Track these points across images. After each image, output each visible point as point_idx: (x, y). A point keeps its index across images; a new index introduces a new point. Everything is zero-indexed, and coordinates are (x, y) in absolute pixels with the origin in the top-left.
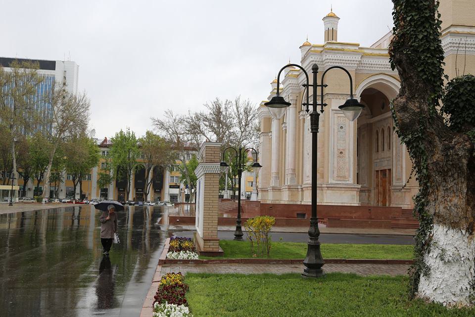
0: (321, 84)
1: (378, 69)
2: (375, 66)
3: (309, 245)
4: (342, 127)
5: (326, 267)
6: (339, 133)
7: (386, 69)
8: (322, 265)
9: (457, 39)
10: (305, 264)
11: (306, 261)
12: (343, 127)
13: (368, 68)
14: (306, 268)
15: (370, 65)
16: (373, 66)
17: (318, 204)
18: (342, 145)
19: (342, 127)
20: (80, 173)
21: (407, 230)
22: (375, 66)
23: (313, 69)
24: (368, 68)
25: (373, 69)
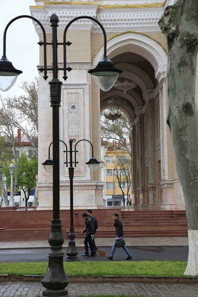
0: (63, 42)
1: (125, 26)
2: (120, 22)
3: (50, 257)
4: (73, 107)
5: (73, 288)
6: (70, 115)
7: (136, 25)
8: (66, 284)
9: (146, 15)
10: (45, 285)
11: (46, 280)
12: (76, 106)
13: (111, 26)
14: (44, 289)
15: (113, 22)
16: (117, 22)
17: (61, 209)
18: (74, 130)
19: (73, 107)
20: (94, 29)
21: (146, 239)
22: (120, 22)
23: (51, 21)
24: (111, 26)
25: (118, 26)
